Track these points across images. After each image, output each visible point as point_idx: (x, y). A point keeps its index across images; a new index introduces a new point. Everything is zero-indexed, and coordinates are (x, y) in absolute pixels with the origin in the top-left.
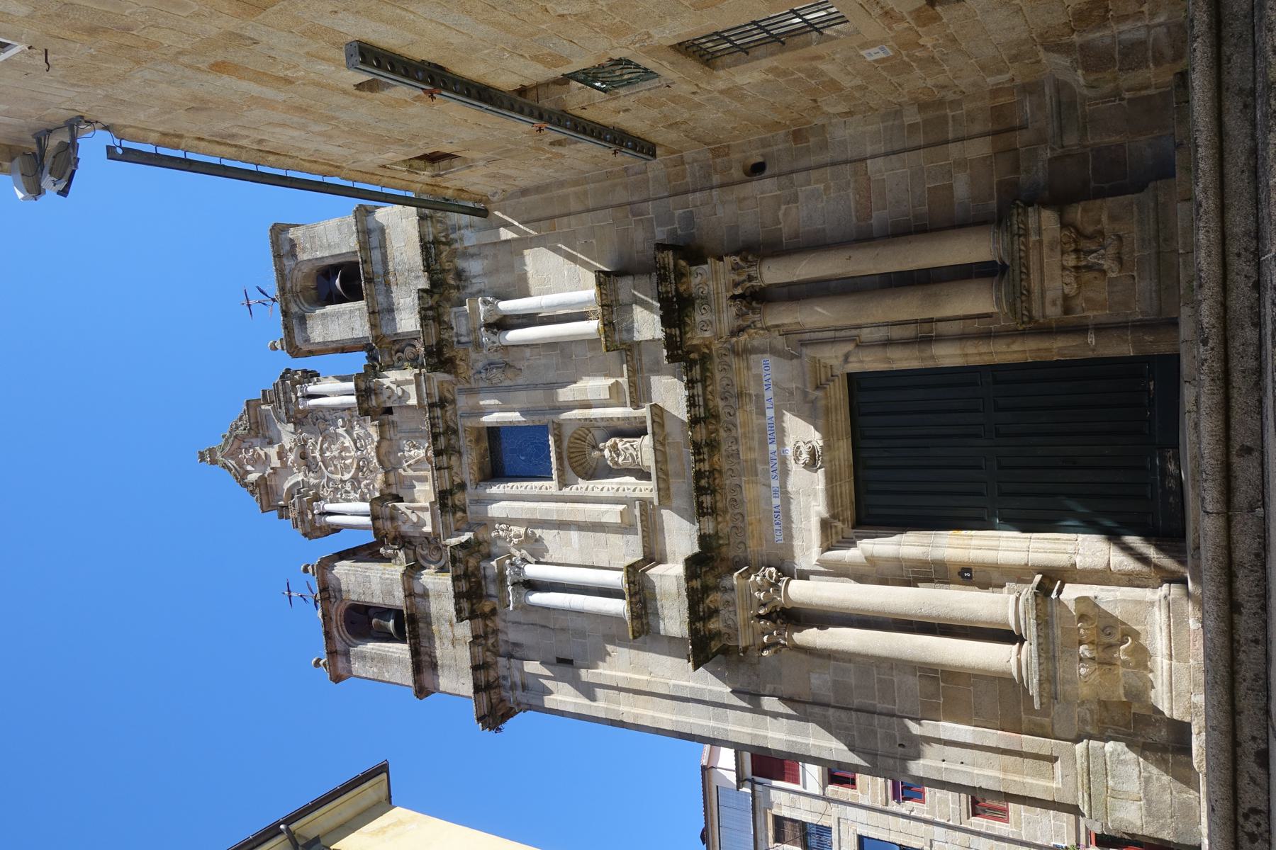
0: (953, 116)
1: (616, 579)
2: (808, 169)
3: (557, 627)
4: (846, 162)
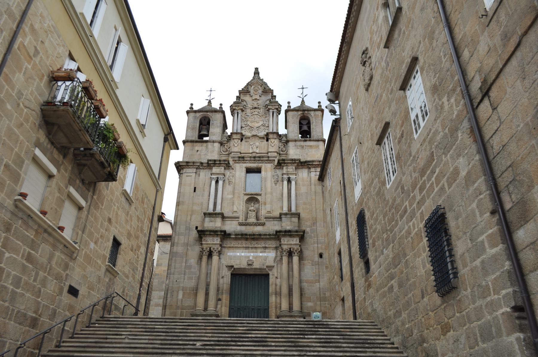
2: (319, 269)
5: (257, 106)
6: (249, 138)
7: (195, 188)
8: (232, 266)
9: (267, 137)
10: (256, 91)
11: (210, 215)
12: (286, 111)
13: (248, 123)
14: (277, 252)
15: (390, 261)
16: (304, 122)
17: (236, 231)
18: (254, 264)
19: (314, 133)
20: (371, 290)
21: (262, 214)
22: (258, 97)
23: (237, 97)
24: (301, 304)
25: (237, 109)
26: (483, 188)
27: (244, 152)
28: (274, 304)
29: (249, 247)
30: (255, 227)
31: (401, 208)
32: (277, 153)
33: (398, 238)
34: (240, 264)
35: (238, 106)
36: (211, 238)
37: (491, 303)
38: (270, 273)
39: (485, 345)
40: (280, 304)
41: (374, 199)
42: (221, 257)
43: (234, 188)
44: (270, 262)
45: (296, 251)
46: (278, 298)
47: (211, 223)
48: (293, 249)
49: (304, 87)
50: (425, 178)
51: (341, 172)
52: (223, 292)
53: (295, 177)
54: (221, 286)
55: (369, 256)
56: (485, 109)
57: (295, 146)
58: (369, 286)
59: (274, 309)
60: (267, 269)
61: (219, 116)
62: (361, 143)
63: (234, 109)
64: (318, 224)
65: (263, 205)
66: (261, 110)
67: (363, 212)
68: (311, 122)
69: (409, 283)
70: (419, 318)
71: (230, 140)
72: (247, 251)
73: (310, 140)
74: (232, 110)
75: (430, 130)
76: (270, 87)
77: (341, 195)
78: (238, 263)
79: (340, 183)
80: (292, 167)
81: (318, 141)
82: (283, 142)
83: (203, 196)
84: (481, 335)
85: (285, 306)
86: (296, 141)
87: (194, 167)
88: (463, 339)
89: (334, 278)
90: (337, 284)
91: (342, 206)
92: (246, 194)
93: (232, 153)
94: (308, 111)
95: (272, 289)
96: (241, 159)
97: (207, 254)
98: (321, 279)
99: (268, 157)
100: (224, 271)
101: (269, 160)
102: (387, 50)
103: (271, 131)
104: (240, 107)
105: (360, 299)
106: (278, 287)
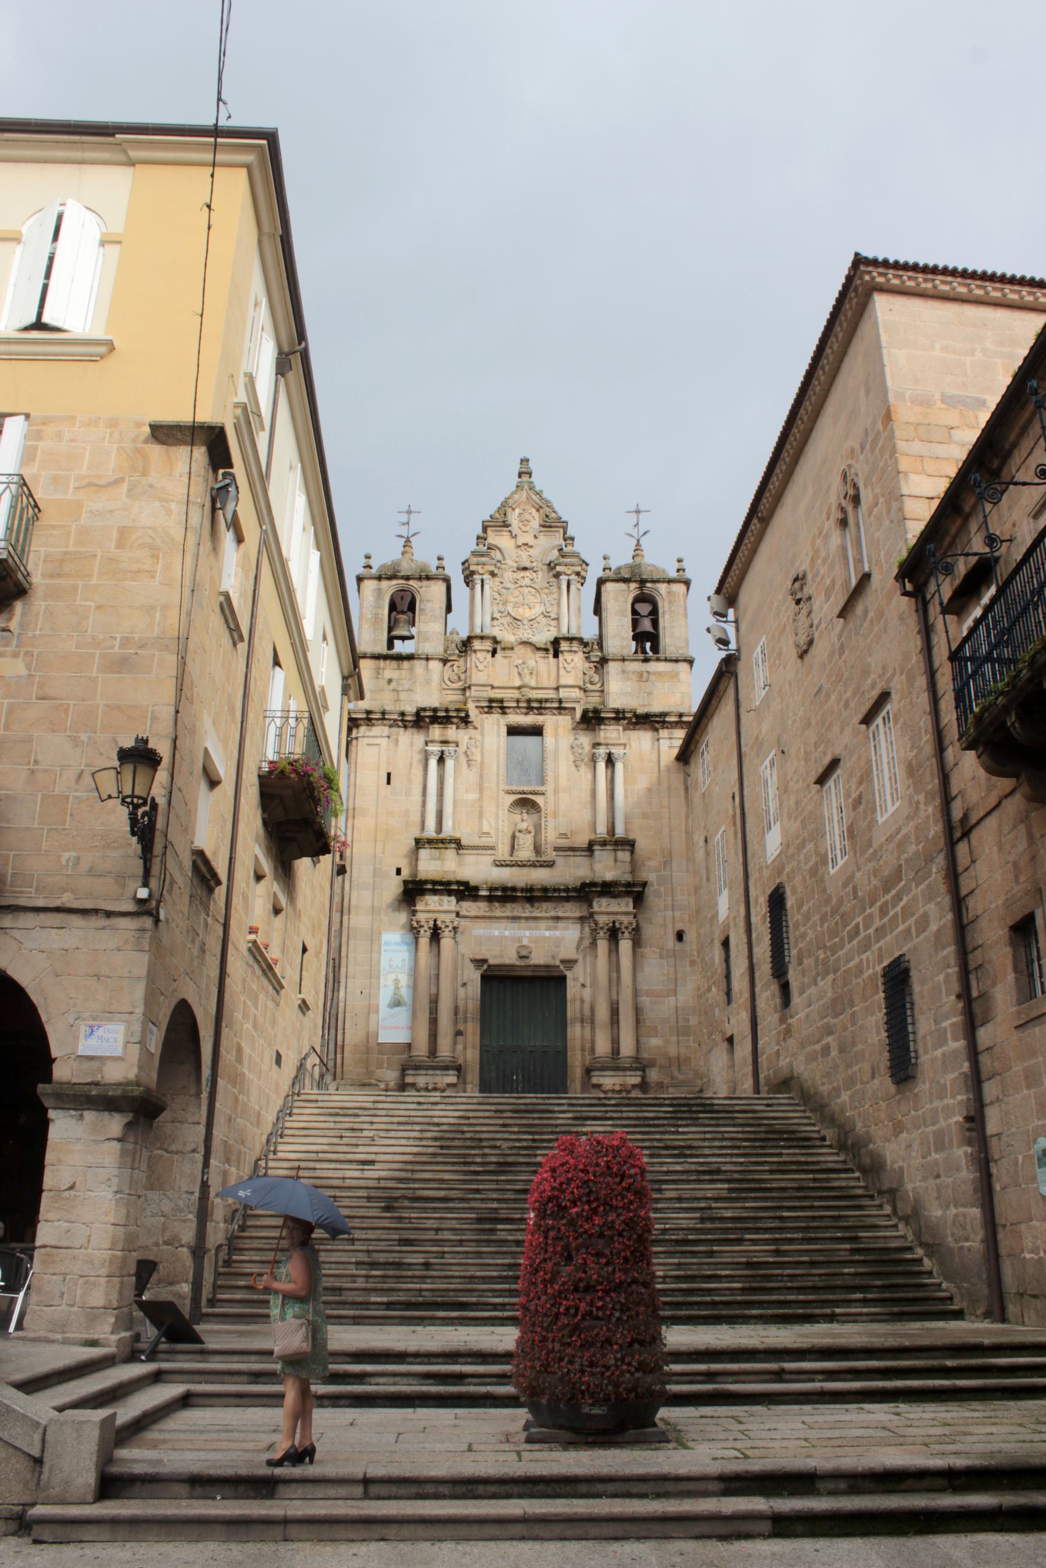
5: (528, 564)
6: (512, 649)
7: (389, 775)
8: (485, 961)
9: (555, 647)
10: (525, 522)
12: (601, 582)
14: (582, 929)
16: (644, 609)
18: (533, 955)
19: (667, 640)
20: (791, 1042)
22: (530, 540)
23: (478, 538)
24: (638, 1041)
25: (481, 571)
26: (952, 961)
28: (578, 1042)
32: (580, 688)
33: (843, 969)
37: (947, 1108)
38: (569, 974)
39: (937, 1156)
40: (593, 1042)
43: (481, 776)
45: (627, 928)
46: (588, 1028)
49: (641, 508)
50: (888, 897)
51: (736, 776)
54: (461, 1004)
56: (962, 848)
57: (624, 672)
58: (788, 1032)
59: (578, 1052)
60: (562, 967)
62: (783, 752)
63: (473, 573)
64: (674, 864)
65: (549, 819)
66: (540, 574)
67: (781, 891)
69: (855, 1049)
70: (867, 1106)
71: (466, 651)
72: (516, 925)
74: (467, 572)
75: (899, 830)
76: (560, 514)
77: (735, 824)
79: (733, 797)
81: (677, 661)
82: (593, 659)
84: (935, 1144)
85: (603, 1047)
87: (385, 722)
88: (916, 1145)
89: (709, 990)
90: (718, 1006)
92: (509, 792)
93: (473, 688)
94: (653, 582)
95: (572, 1010)
96: (495, 706)
97: (428, 934)
98: (679, 989)
99: (560, 701)
100: (466, 972)
102: (842, 620)
103: (564, 631)
105: (768, 1051)
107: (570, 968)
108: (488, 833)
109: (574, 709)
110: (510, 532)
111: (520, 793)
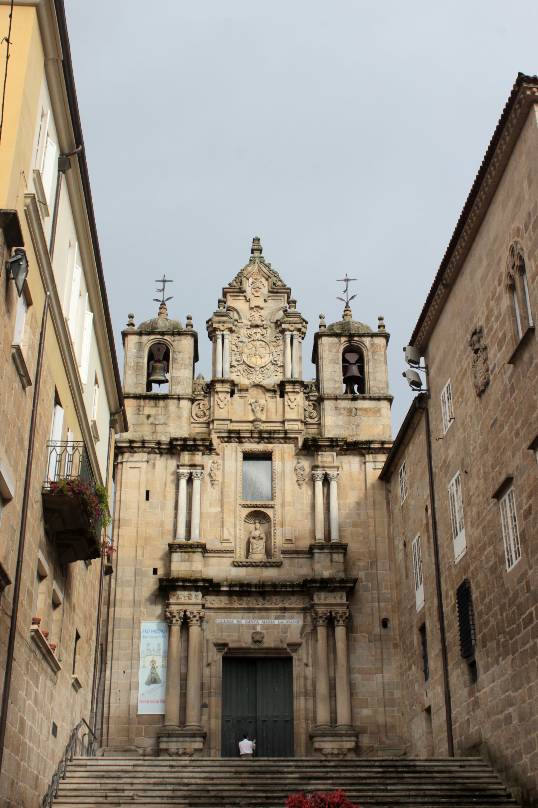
0: (394, 710)
1: (196, 537)
2: (382, 648)
3: (166, 493)
4: (382, 665)
5: (259, 323)
6: (247, 390)
7: (148, 492)
8: (226, 645)
10: (257, 289)
11: (182, 548)
12: (318, 337)
13: (245, 357)
15: (508, 679)
16: (352, 358)
17: (229, 577)
18: (265, 640)
20: (479, 712)
21: (277, 544)
22: (262, 304)
23: (220, 301)
24: (352, 712)
25: (222, 328)
27: (238, 419)
28: (303, 712)
29: (254, 609)
30: (264, 569)
31: (526, 612)
32: (302, 422)
34: (239, 641)
35: (224, 323)
36: (186, 593)
38: (295, 656)
40: (315, 712)
41: (486, 575)
42: (203, 627)
43: (222, 493)
44: (294, 636)
45: (341, 617)
47: (183, 563)
48: (336, 613)
52: (210, 693)
53: (335, 473)
54: (206, 681)
55: (476, 657)
57: (336, 408)
58: (476, 704)
60: (288, 650)
61: (187, 343)
64: (379, 563)
66: (269, 330)
67: (467, 586)
68: (365, 359)
72: (251, 615)
73: (364, 399)
74: (211, 329)
77: (428, 531)
78: (235, 638)
80: (330, 453)
81: (379, 399)
82: (312, 398)
83: (163, 508)
86: (336, 399)
87: (145, 450)
90: (417, 681)
91: (429, 552)
92: (245, 506)
93: (216, 422)
95: (298, 685)
97: (179, 622)
98: (385, 667)
99: (286, 432)
101: (286, 439)
103: (289, 376)
104: (227, 325)
105: (460, 720)
106: (309, 682)
107: (295, 651)
108: (228, 540)
109: (297, 438)
110: (245, 296)
111: (254, 507)
